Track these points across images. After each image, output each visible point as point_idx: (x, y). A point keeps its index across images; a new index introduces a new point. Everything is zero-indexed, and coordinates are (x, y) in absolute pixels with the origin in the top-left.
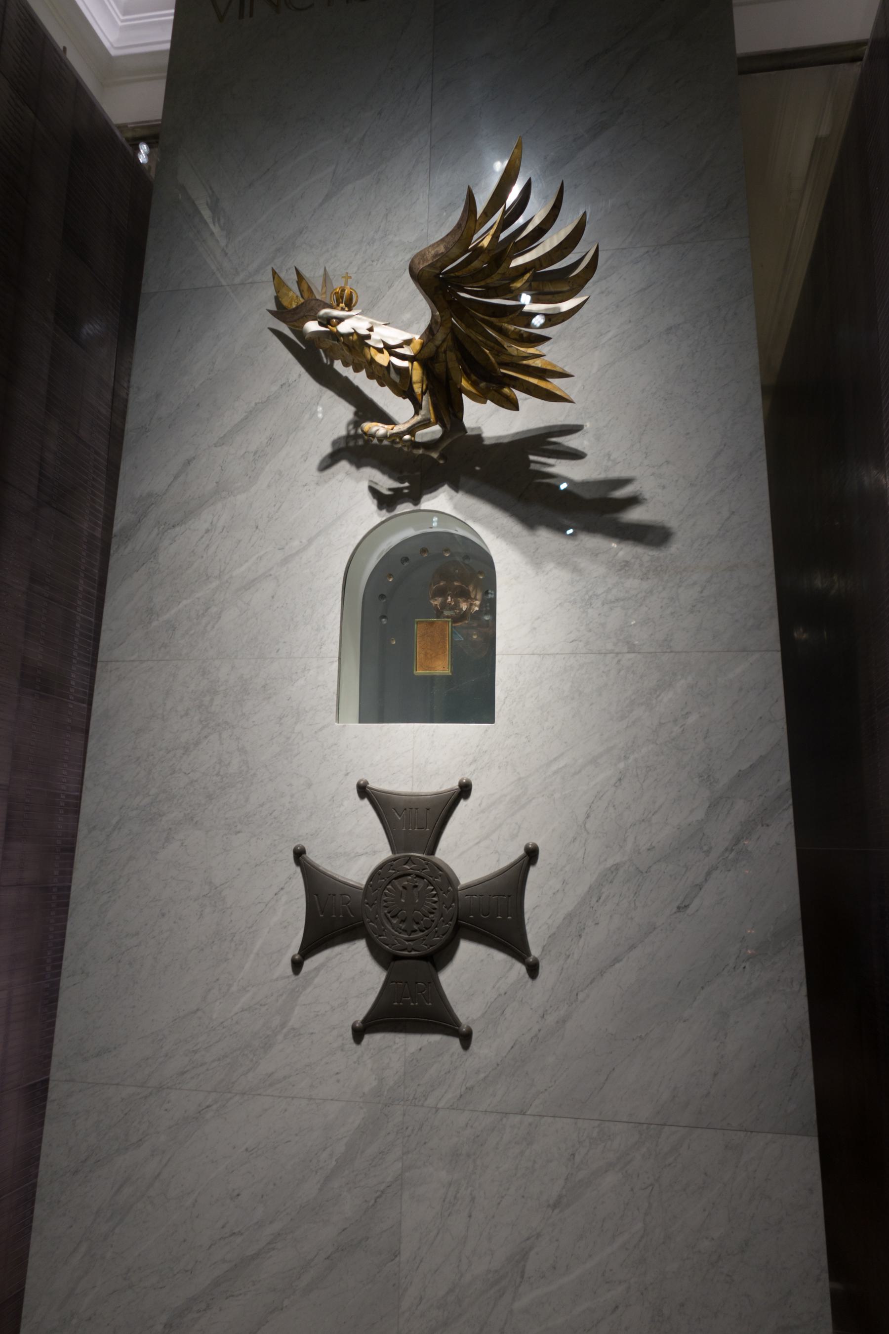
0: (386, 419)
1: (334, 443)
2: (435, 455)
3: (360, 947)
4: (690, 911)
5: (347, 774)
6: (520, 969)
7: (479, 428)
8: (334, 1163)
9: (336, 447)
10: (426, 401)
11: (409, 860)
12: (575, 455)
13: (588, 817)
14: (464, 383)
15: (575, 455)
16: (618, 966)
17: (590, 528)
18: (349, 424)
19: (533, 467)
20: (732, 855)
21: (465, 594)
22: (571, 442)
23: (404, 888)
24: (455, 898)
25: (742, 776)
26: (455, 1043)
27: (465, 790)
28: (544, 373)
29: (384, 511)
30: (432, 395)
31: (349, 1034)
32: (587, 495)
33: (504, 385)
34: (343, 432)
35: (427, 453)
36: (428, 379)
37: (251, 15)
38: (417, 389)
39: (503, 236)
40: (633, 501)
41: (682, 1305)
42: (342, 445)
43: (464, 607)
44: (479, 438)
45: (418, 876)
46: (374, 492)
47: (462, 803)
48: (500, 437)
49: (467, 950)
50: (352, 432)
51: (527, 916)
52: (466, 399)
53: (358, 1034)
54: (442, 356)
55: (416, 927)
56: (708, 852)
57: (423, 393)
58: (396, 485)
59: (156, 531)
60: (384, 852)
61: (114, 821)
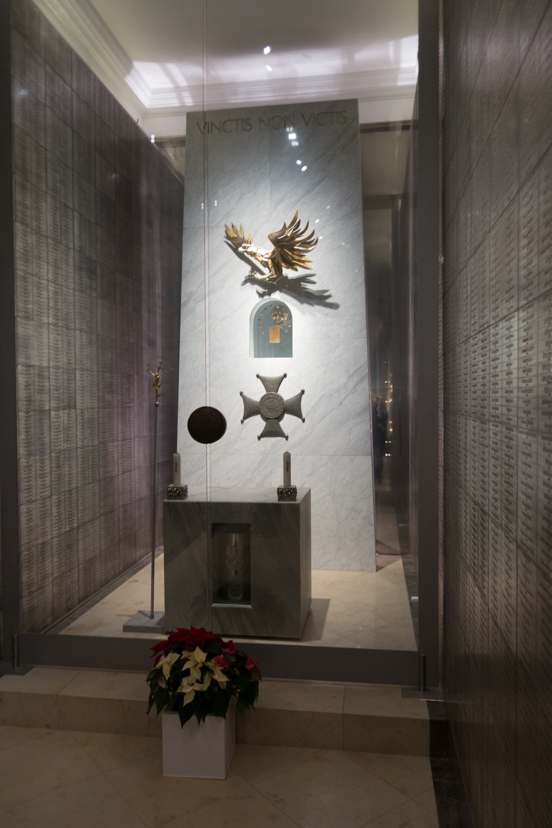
0: (262, 273)
1: (246, 277)
2: (275, 283)
3: (259, 417)
4: (343, 404)
5: (253, 372)
6: (300, 420)
7: (287, 274)
8: (254, 469)
9: (246, 279)
10: (273, 269)
11: (271, 394)
12: (314, 283)
13: (317, 382)
14: (283, 264)
15: (314, 283)
16: (325, 419)
17: (318, 304)
18: (249, 272)
19: (302, 286)
20: (353, 391)
21: (282, 316)
22: (312, 279)
23: (270, 401)
24: (283, 403)
25: (356, 371)
26: (284, 439)
27: (285, 376)
28: (304, 262)
29: (261, 298)
30: (274, 268)
31: (257, 438)
32: (317, 294)
33: (294, 265)
34: (248, 274)
35: (273, 282)
36: (273, 263)
37: (212, 132)
38: (270, 266)
39: (294, 232)
40: (329, 296)
41: (339, 495)
42: (248, 278)
43: (282, 319)
44: (287, 277)
45: (273, 398)
46: (258, 293)
47: (285, 379)
48: (293, 277)
49: (287, 416)
50: (251, 274)
51: (302, 408)
52: (283, 268)
53: (259, 438)
54: (277, 258)
55: (273, 411)
56: (347, 390)
57: (272, 267)
58: (264, 290)
59: (194, 303)
60: (264, 392)
61: (189, 386)
